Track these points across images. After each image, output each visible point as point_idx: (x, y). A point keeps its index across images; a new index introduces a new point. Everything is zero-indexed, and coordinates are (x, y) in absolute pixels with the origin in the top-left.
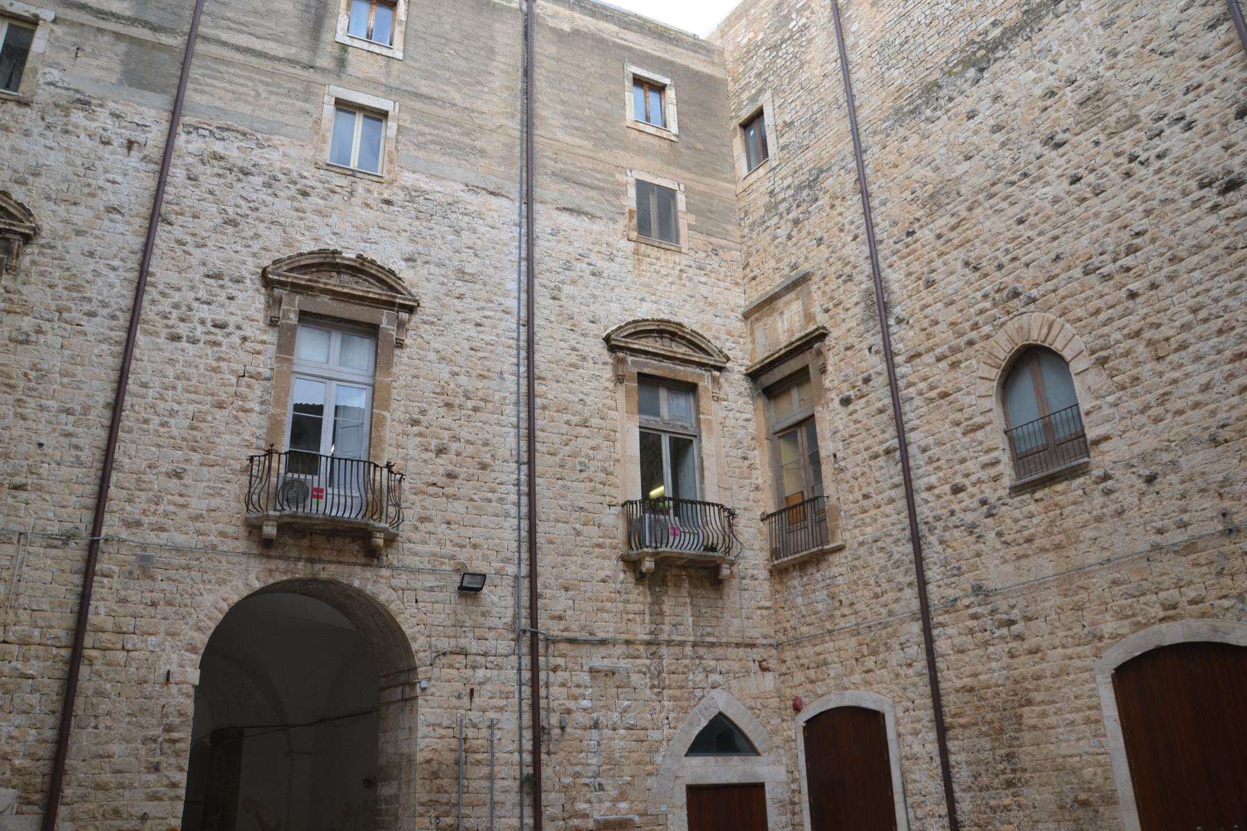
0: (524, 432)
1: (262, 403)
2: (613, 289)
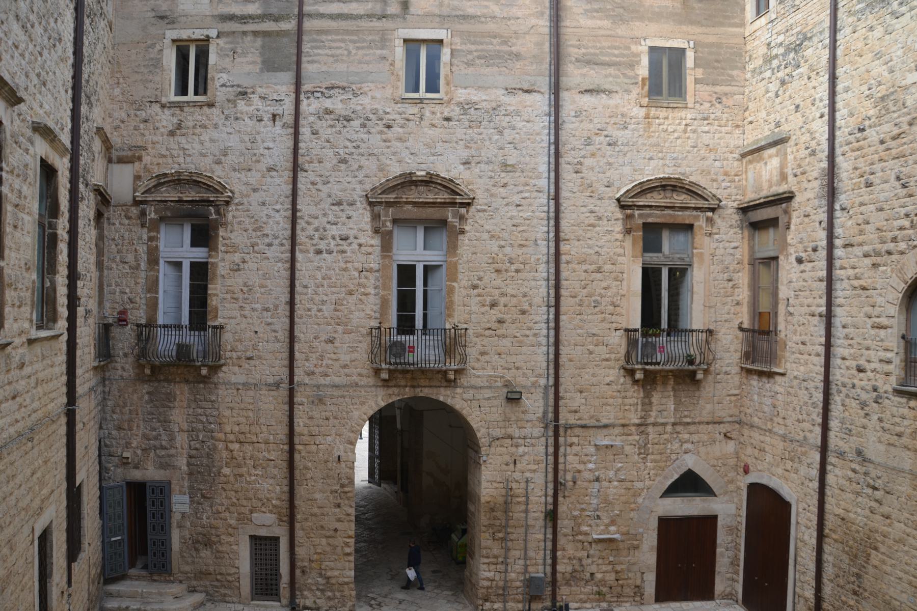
0: (552, 282)
1: (375, 288)
2: (625, 154)
